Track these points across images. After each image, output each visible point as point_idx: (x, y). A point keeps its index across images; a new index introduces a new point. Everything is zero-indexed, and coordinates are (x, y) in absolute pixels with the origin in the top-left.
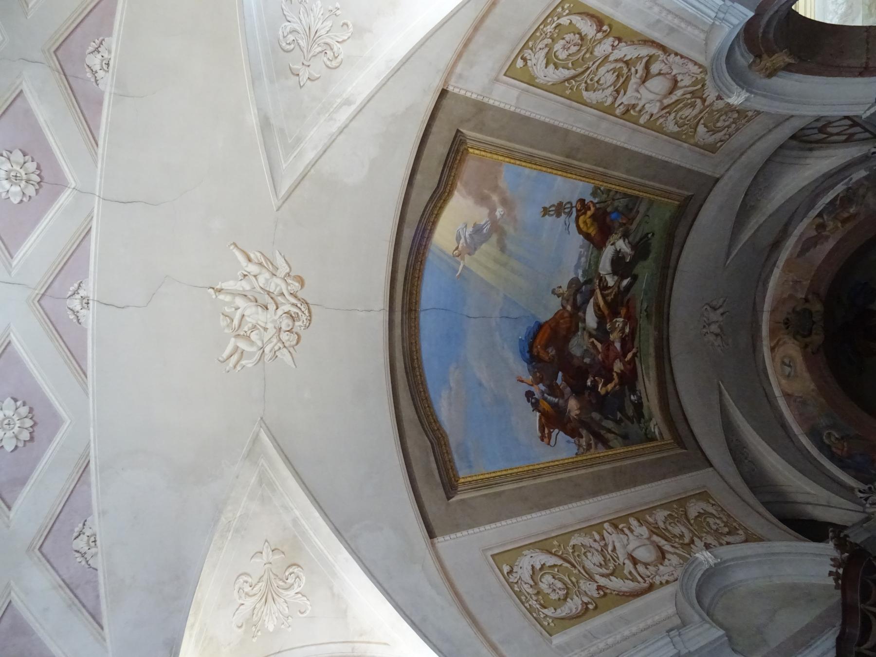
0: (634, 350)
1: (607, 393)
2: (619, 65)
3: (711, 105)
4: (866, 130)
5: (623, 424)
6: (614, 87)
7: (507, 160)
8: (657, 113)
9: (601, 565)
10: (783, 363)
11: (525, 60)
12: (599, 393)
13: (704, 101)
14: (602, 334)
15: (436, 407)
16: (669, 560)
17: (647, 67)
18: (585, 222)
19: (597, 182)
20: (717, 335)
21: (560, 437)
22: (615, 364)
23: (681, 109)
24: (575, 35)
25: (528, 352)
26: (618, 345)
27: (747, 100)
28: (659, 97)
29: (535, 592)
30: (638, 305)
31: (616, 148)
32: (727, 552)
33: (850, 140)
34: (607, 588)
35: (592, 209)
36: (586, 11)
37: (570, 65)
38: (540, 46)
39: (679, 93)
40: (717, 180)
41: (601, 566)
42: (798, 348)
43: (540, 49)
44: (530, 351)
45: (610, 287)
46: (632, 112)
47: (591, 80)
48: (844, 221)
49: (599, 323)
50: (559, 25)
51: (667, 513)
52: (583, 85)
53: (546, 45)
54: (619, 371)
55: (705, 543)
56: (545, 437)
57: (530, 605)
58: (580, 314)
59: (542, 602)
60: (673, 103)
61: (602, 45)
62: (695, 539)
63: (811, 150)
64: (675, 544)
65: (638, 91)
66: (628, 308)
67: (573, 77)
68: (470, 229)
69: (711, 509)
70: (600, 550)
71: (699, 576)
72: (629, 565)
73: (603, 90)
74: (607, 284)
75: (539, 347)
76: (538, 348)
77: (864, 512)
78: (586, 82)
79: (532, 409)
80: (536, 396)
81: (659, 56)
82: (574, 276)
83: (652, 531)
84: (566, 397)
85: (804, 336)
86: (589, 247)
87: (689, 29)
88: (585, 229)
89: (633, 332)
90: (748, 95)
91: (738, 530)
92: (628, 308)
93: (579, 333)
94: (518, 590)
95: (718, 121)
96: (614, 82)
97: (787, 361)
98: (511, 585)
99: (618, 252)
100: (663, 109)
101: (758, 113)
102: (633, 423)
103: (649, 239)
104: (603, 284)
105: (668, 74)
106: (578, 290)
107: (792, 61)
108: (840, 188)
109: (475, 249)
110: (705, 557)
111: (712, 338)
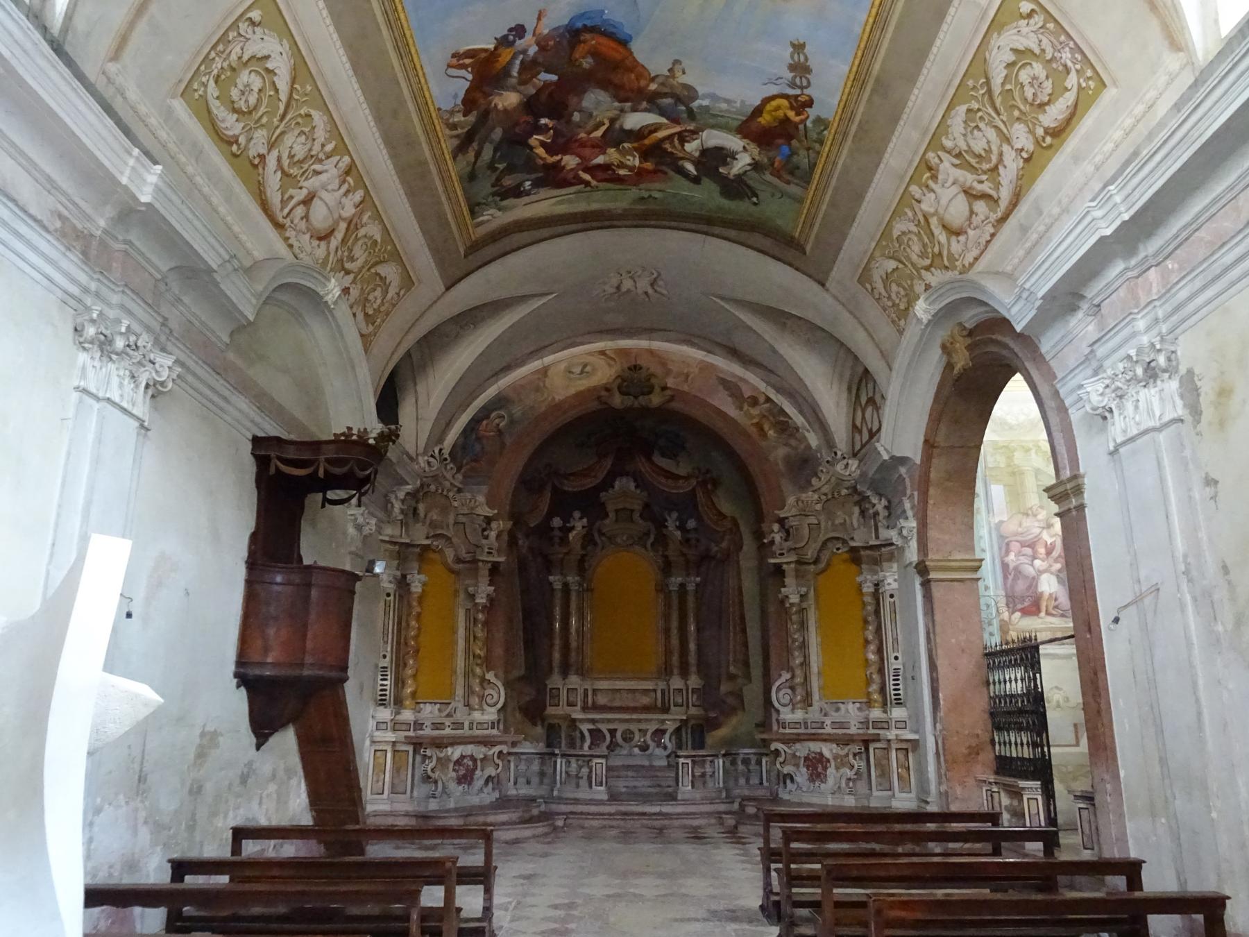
0: (594, 183)
1: (531, 148)
2: (994, 158)
3: (921, 278)
4: (863, 446)
5: (489, 172)
6: (965, 151)
8: (921, 210)
9: (293, 156)
10: (585, 366)
11: (1030, 15)
12: (531, 136)
13: (927, 268)
14: (616, 137)
16: (319, 246)
17: (984, 196)
18: (778, 108)
19: (835, 125)
20: (618, 288)
21: (461, 84)
22: (573, 156)
23: (921, 239)
24: (1050, 95)
25: (585, 26)
26: (600, 160)
27: (919, 321)
28: (941, 211)
29: (234, 65)
30: (657, 185)
31: (879, 153)
32: (343, 313)
33: (855, 429)
34: (264, 169)
35: (797, 119)
36: (1078, 112)
37: (1008, 87)
38: (1045, 41)
39: (942, 237)
40: (823, 285)
41: (291, 157)
42: (604, 381)
43: (1040, 41)
44: (586, 29)
45: (683, 146)
46: (928, 175)
47: (981, 118)
48: (759, 427)
49: (630, 132)
50: (1068, 71)
51: (378, 237)
52: (975, 106)
53: (1043, 51)
54: (563, 164)
55: (349, 288)
56: (458, 60)
57: (214, 59)
58: (644, 104)
59: (223, 77)
60: (931, 230)
61: (1026, 135)
62: (352, 276)
63: (849, 389)
64: (339, 253)
65: (954, 184)
66: (655, 172)
67: (990, 92)
69: (392, 292)
70: (313, 153)
71: (309, 284)
72: (301, 195)
73: (964, 135)
74: (688, 142)
75: (593, 42)
76: (592, 41)
77: (417, 455)
78: (979, 110)
80: (518, 42)
81: (995, 212)
82: (700, 94)
83: (351, 221)
84: (522, 88)
85: (619, 388)
87: (1021, 253)
88: (768, 107)
89: (620, 180)
90: (925, 321)
91: (373, 324)
92: (655, 172)
93: (616, 104)
94: (231, 38)
95: (899, 285)
96: (973, 152)
97: (588, 369)
98: (234, 25)
99: (733, 155)
100: (924, 216)
101: (901, 332)
102: (493, 186)
103: (749, 199)
105: (971, 223)
106: (679, 100)
107: (956, 371)
108: (799, 420)
110: (332, 289)
111: (615, 282)
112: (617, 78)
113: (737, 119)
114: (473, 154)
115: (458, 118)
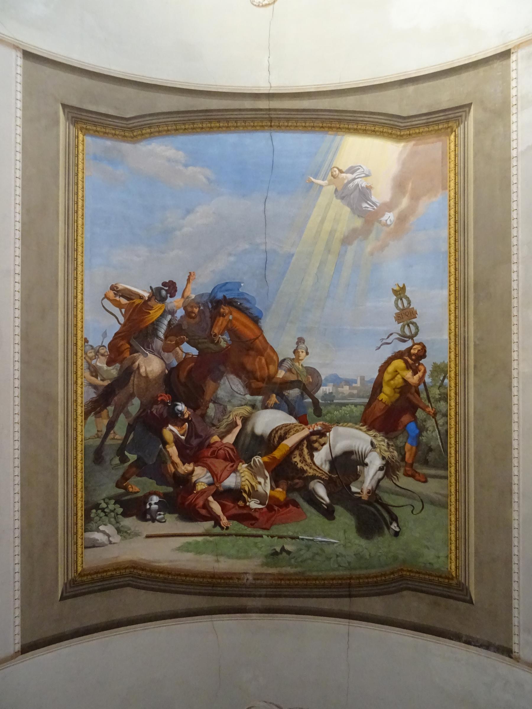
0: (224, 521)
1: (165, 443)
7: (452, 194)
15: (168, 140)
19: (453, 365)
26: (231, 481)
30: (290, 529)
40: (507, 652)
45: (312, 456)
66: (286, 504)
68: (362, 182)
79: (154, 287)
80: (169, 300)
84: (166, 355)
86: (363, 397)
88: (387, 377)
93: (248, 397)
104: (316, 441)
109: (342, 198)
112: (250, 362)
113: (360, 404)
114: (106, 422)
115: (101, 363)
